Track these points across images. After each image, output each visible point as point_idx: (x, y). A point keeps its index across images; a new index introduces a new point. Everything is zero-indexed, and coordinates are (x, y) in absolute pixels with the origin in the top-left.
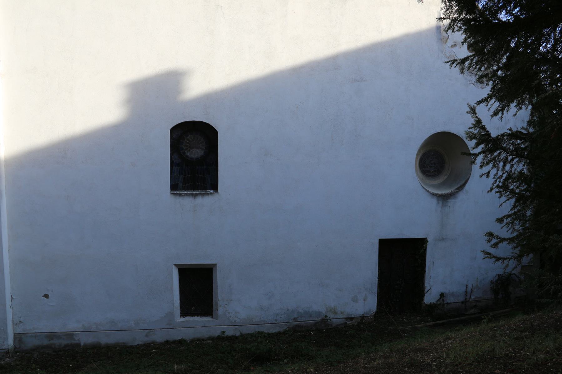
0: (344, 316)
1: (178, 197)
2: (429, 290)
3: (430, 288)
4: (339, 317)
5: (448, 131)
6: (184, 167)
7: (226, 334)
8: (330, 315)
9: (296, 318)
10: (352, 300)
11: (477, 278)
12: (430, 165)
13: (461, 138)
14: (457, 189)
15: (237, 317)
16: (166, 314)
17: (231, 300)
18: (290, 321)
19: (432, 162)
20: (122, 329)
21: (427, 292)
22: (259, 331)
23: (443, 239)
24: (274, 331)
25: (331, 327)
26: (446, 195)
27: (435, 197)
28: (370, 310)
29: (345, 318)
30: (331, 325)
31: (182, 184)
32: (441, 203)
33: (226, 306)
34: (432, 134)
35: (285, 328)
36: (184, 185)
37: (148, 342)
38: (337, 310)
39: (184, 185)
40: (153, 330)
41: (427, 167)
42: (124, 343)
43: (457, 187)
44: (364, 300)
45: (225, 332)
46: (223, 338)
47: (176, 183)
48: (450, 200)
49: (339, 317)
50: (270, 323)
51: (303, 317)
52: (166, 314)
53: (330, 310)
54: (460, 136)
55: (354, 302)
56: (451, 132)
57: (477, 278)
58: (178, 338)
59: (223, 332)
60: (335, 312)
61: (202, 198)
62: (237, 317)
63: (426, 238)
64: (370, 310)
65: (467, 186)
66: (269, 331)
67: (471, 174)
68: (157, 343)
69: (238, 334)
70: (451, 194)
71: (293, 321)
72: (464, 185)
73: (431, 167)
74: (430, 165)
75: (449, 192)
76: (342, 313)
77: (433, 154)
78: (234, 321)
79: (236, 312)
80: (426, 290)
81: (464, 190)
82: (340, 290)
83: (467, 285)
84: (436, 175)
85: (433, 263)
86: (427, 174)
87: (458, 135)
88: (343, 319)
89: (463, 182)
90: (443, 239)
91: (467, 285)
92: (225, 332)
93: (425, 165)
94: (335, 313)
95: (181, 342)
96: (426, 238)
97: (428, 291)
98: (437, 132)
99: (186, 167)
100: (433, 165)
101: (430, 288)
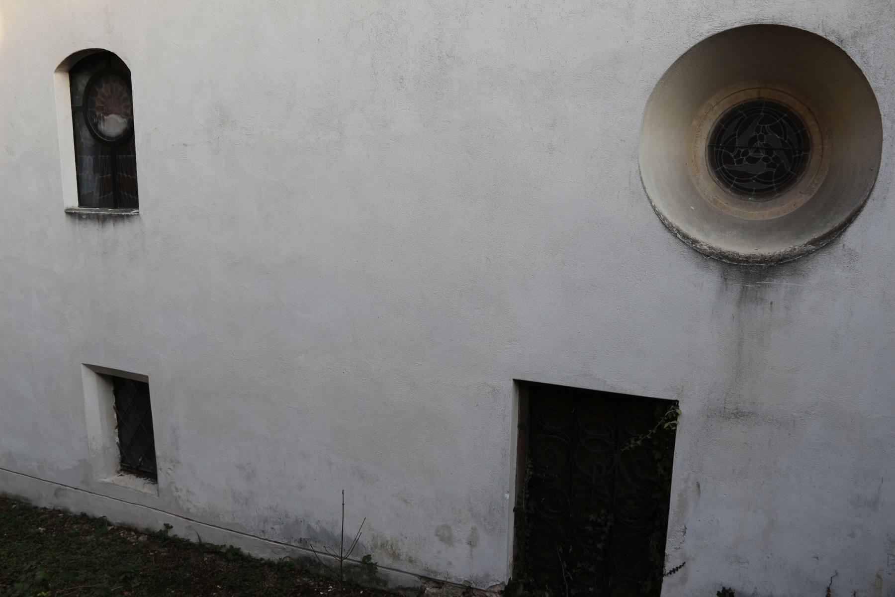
0: (418, 571)
1: (77, 221)
2: (677, 569)
3: (684, 563)
4: (406, 571)
5: (777, 22)
6: (100, 156)
7: (171, 534)
8: (381, 559)
9: (304, 539)
10: (437, 535)
11: (879, 576)
12: (751, 154)
13: (824, 38)
14: (814, 242)
15: (191, 503)
16: (79, 461)
17: (178, 462)
18: (291, 544)
19: (759, 144)
20: (23, 473)
21: (670, 573)
22: (233, 545)
23: (738, 415)
24: (261, 556)
25: (384, 588)
26: (764, 260)
27: (712, 264)
28: (487, 576)
29: (422, 577)
30: (385, 583)
31: (98, 195)
32: (735, 288)
33: (170, 471)
34: (706, 35)
35: (283, 556)
36: (102, 197)
37: (59, 508)
38: (399, 550)
39: (102, 197)
40: (64, 487)
41: (740, 162)
42: (27, 499)
43: (816, 235)
44: (470, 544)
45: (172, 527)
46: (166, 539)
47: (90, 191)
48: (775, 282)
49: (403, 569)
50: (252, 533)
51: (319, 542)
52: (79, 461)
53: (383, 545)
54: (832, 39)
55: (441, 540)
56: (791, 24)
57: (879, 576)
58: (99, 514)
59: (168, 527)
60: (394, 552)
61: (102, 226)
62: (191, 503)
63: (675, 403)
64: (487, 576)
65: (852, 231)
66: (251, 552)
67: (873, 186)
68: (70, 513)
69: (194, 539)
70: (781, 260)
71: (298, 545)
72: (841, 229)
73: (752, 160)
74: (751, 154)
75: (782, 250)
76: (411, 561)
77: (762, 114)
78: (186, 509)
79: (188, 491)
80: (668, 567)
81: (838, 250)
82: (405, 501)
83: (829, 589)
84: (772, 188)
85: (698, 486)
86: (735, 185)
87: (820, 33)
88: (416, 578)
89: (841, 219)
90: (738, 415)
91: (829, 589)
92: (172, 527)
93: (732, 155)
94: (396, 556)
95: (102, 522)
96: (675, 403)
97: (674, 571)
98: (729, 27)
99: (103, 156)
100: (762, 155)
101: (684, 563)
